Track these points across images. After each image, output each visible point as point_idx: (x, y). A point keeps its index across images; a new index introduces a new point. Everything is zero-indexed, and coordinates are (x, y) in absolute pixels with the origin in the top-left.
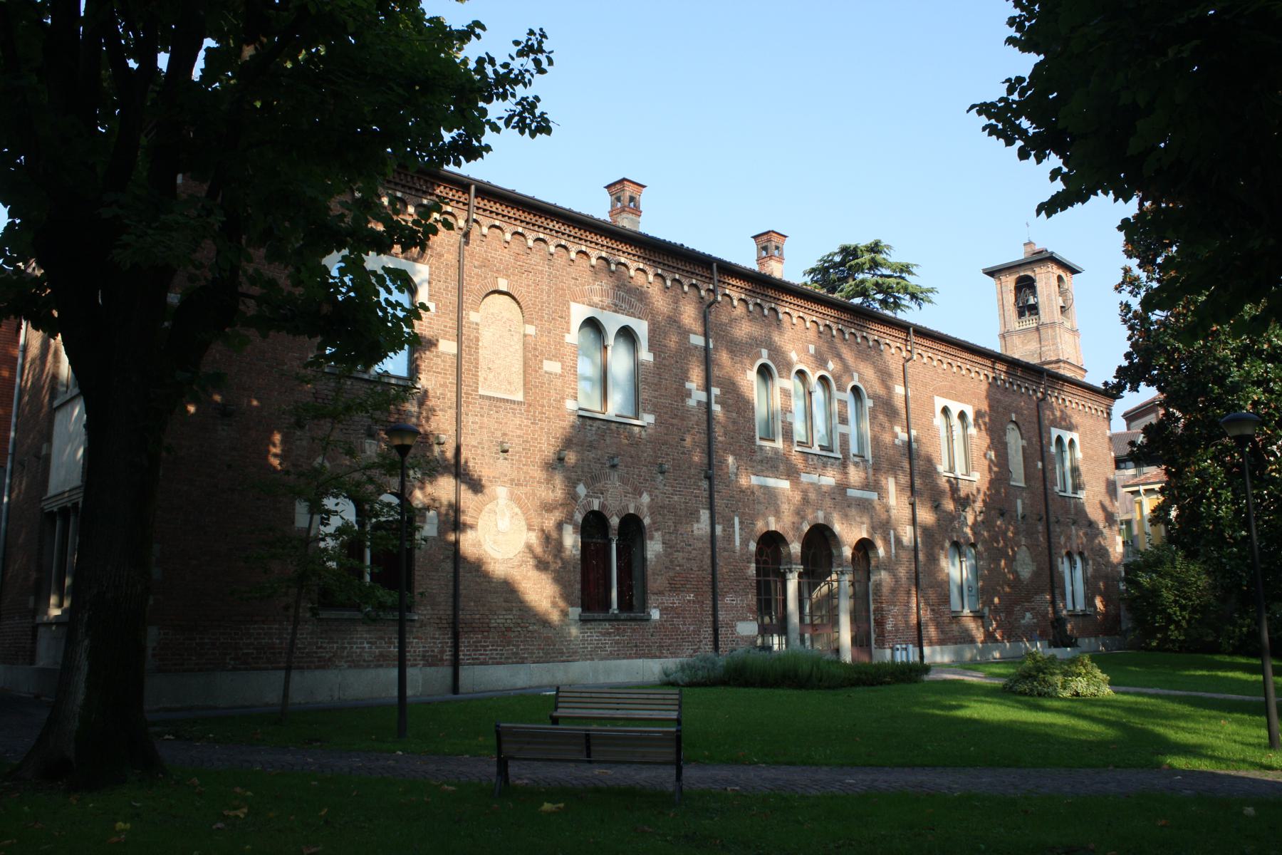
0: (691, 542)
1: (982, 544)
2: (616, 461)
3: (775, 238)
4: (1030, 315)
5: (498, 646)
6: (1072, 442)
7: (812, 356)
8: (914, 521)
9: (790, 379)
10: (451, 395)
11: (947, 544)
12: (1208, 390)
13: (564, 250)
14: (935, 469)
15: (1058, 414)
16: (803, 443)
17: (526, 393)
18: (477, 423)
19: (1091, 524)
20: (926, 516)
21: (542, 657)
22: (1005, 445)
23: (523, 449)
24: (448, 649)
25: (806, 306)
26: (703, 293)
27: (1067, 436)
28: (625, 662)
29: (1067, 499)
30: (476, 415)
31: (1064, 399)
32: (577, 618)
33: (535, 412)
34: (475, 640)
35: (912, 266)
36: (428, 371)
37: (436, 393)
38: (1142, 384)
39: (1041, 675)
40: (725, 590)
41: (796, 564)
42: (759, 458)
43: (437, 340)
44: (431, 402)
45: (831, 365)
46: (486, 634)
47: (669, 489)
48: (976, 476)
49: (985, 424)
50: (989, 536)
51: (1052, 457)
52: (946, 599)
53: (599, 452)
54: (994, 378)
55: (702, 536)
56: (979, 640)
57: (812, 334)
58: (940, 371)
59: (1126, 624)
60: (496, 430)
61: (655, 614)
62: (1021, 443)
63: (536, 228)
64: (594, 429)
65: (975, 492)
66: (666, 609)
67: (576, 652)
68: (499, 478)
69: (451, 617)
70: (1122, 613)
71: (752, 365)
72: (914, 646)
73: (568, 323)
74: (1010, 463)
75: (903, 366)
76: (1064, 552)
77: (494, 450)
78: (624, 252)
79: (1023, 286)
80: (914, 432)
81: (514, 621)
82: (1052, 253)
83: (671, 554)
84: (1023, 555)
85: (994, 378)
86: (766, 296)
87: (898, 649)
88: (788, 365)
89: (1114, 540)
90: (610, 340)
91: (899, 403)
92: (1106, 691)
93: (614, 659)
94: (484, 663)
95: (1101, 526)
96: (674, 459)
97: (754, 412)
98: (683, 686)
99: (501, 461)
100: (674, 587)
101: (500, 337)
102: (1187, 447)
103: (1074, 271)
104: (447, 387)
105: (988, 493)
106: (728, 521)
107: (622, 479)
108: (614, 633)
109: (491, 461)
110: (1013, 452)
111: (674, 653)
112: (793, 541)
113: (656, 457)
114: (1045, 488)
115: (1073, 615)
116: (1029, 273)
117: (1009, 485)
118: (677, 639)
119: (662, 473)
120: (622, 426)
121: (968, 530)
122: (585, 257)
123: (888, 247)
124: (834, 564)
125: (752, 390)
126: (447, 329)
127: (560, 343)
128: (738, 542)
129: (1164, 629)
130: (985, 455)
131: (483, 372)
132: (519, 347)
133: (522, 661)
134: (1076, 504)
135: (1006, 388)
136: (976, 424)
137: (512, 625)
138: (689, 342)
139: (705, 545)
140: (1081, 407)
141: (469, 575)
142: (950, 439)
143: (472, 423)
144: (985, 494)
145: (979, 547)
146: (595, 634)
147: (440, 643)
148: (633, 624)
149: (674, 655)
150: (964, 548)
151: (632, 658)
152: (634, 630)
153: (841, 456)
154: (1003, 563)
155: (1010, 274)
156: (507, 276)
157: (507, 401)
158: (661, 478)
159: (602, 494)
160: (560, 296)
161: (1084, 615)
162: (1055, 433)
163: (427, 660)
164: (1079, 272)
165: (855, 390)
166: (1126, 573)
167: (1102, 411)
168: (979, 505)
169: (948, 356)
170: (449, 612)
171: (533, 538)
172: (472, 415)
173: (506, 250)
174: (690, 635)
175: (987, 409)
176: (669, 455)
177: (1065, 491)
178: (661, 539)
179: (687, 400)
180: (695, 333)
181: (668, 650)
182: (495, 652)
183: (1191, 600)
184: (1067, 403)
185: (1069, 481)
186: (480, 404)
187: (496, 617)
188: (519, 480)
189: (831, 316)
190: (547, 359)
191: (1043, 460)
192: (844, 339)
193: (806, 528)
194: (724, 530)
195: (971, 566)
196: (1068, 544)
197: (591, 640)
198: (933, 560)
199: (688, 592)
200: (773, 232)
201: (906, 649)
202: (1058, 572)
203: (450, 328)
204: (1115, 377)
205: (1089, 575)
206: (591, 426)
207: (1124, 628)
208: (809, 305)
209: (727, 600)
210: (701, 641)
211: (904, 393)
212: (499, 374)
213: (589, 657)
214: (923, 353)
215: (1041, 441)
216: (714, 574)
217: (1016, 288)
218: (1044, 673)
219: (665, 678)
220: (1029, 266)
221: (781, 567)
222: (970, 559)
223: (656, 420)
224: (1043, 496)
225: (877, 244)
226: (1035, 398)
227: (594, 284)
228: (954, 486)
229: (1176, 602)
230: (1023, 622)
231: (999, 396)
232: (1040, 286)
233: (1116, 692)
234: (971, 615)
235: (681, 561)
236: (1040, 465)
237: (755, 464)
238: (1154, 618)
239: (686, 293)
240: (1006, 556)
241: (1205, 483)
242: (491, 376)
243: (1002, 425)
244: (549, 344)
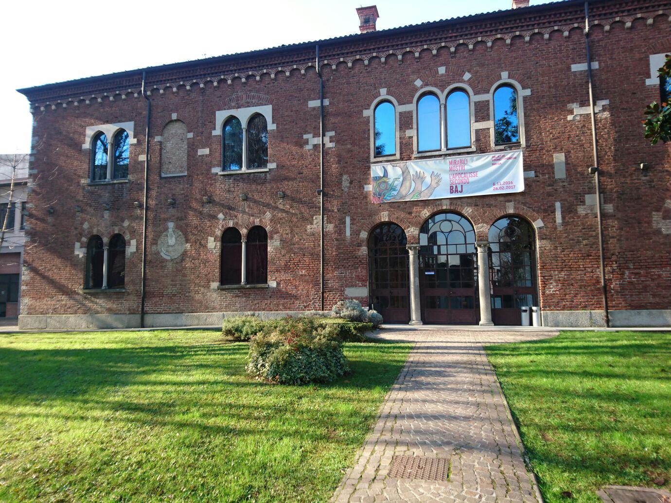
127: (210, 136)
242: (171, 166)
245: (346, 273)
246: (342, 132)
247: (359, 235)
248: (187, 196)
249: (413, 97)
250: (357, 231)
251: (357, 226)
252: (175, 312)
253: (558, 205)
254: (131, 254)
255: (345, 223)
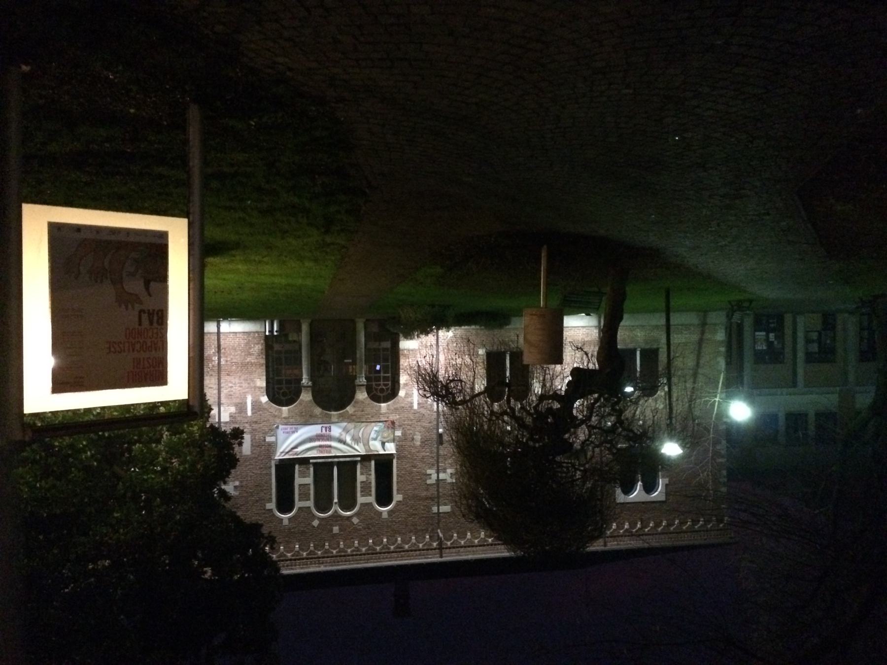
249: (639, 490)
252: (570, 328)
253: (249, 413)
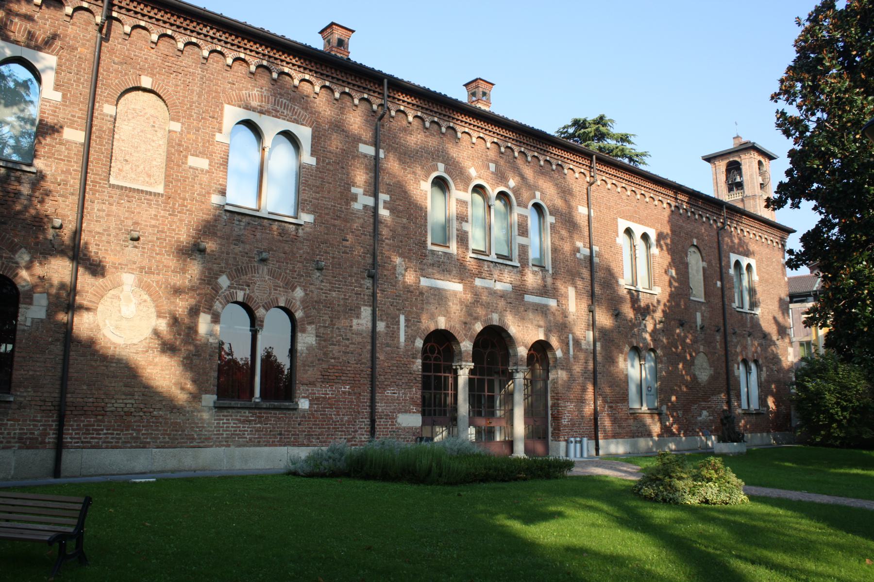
0: (349, 335)
1: (661, 349)
2: (264, 255)
3: (482, 85)
4: (738, 190)
5: (114, 430)
6: (749, 266)
7: (492, 173)
8: (593, 325)
9: (467, 192)
10: (75, 182)
11: (627, 349)
12: (864, 190)
13: (221, 56)
14: (617, 282)
15: (736, 241)
16: (483, 252)
17: (166, 186)
18: (104, 211)
19: (765, 336)
20: (604, 319)
21: (168, 442)
22: (686, 265)
23: (158, 239)
24: (51, 432)
25: (487, 127)
26: (375, 107)
27: (745, 262)
28: (267, 449)
29: (744, 315)
30: (104, 203)
31: (742, 230)
32: (212, 405)
33: (174, 204)
34: (86, 423)
35: (630, 135)
36: (48, 157)
37: (56, 179)
38: (803, 200)
39: (667, 479)
40: (386, 383)
41: (467, 361)
42: (430, 261)
43: (62, 127)
44: (48, 185)
45: (512, 183)
46: (100, 417)
47: (326, 285)
48: (657, 290)
49: (667, 245)
50: (668, 343)
51: (731, 278)
52: (624, 397)
53: (248, 247)
54: (676, 206)
55: (362, 331)
56: (655, 434)
57: (492, 154)
58: (624, 197)
59: (796, 422)
60: (127, 218)
61: (304, 404)
62: (702, 264)
63: (188, 32)
64: (242, 224)
65: (655, 304)
66: (317, 399)
67: (209, 438)
68: (127, 265)
69: (57, 399)
70: (793, 413)
71: (427, 176)
72: (590, 438)
73: (220, 123)
74: (690, 280)
75: (587, 189)
76: (740, 359)
77: (123, 237)
78: (288, 63)
79: (732, 169)
80: (596, 248)
81: (135, 405)
82: (754, 143)
83: (326, 347)
84: (702, 361)
85: (676, 206)
86: (445, 115)
87: (572, 442)
88: (467, 179)
89: (786, 350)
90: (268, 141)
91: (583, 222)
92: (740, 499)
93: (254, 446)
94: (96, 447)
95: (775, 338)
96: (333, 258)
97: (426, 219)
98: (302, 476)
99: (130, 248)
100: (326, 379)
101: (142, 131)
102: (842, 250)
103: (771, 157)
104: (71, 174)
105: (668, 304)
106: (392, 318)
107: (271, 273)
108: (255, 421)
109: (118, 248)
110: (694, 272)
111: (325, 442)
112: (464, 340)
113: (314, 254)
114: (723, 304)
115: (747, 413)
116: (737, 159)
117: (690, 299)
118: (329, 428)
119: (320, 269)
120: (276, 223)
121: (648, 337)
122: (244, 65)
123: (612, 121)
124: (511, 363)
125: (426, 199)
126: (75, 119)
128: (402, 338)
129: (828, 427)
130: (666, 272)
131: (118, 163)
132: (163, 142)
133: (144, 446)
134: (752, 318)
135: (689, 217)
136: (659, 245)
137: (133, 410)
138: (358, 151)
139: (365, 340)
140: (758, 238)
141: (82, 358)
142: (634, 258)
143: (98, 210)
144: (665, 305)
145: (659, 352)
146: (231, 422)
147: (41, 425)
148: (278, 412)
149: (324, 443)
150: (644, 353)
151: (276, 446)
152: (279, 419)
153: (519, 265)
154: (681, 366)
155: (722, 160)
156: (152, 75)
157: (142, 191)
158: (318, 274)
159: (248, 286)
160: (212, 98)
161: (758, 414)
162: (734, 258)
163: (24, 443)
164: (775, 158)
165: (537, 207)
166: (797, 378)
167: (777, 242)
168: (659, 315)
169: (632, 184)
170: (56, 395)
171: (163, 325)
172: (98, 203)
173: (152, 51)
174: (344, 425)
175: (669, 232)
176: (329, 253)
177: (742, 308)
178: (314, 332)
179: (352, 203)
180: (365, 143)
181: (318, 439)
182: (110, 436)
183: (851, 402)
184: (746, 234)
185: (747, 298)
186: (108, 193)
187: (113, 401)
188: (150, 268)
189: (513, 140)
190: (193, 155)
191: (721, 280)
192: (527, 161)
193: (479, 327)
194: (387, 327)
195: (650, 367)
196: (744, 353)
197: (228, 427)
198: (611, 360)
199: (344, 383)
200: (481, 79)
201: (581, 442)
202: (734, 376)
203: (79, 117)
204: (776, 192)
205: (763, 380)
206: (240, 221)
207: (793, 425)
208: (489, 127)
209: (388, 393)
210: (356, 431)
211: (587, 213)
212: (138, 166)
213: (224, 443)
214: (607, 180)
215: (720, 264)
216: (373, 368)
217: (727, 170)
218: (671, 477)
219: (292, 467)
220: (736, 154)
221: (453, 364)
222: (649, 361)
223: (315, 220)
224: (721, 311)
225: (602, 118)
226: (715, 227)
227: (253, 90)
228: (634, 297)
229: (837, 403)
230: (699, 418)
231: (681, 222)
232: (744, 168)
233: (752, 498)
234: (648, 412)
235: (336, 355)
236: (719, 284)
237: (425, 267)
238: (818, 417)
239: (356, 106)
240: (684, 360)
241: (860, 285)
242: (127, 167)
243: (683, 247)
244: (196, 141)
245: (399, 393)
246: (397, 199)
247: (414, 342)
248: (163, 232)
250: (412, 336)
251: (412, 330)
254: (32, 322)
255: (399, 325)
